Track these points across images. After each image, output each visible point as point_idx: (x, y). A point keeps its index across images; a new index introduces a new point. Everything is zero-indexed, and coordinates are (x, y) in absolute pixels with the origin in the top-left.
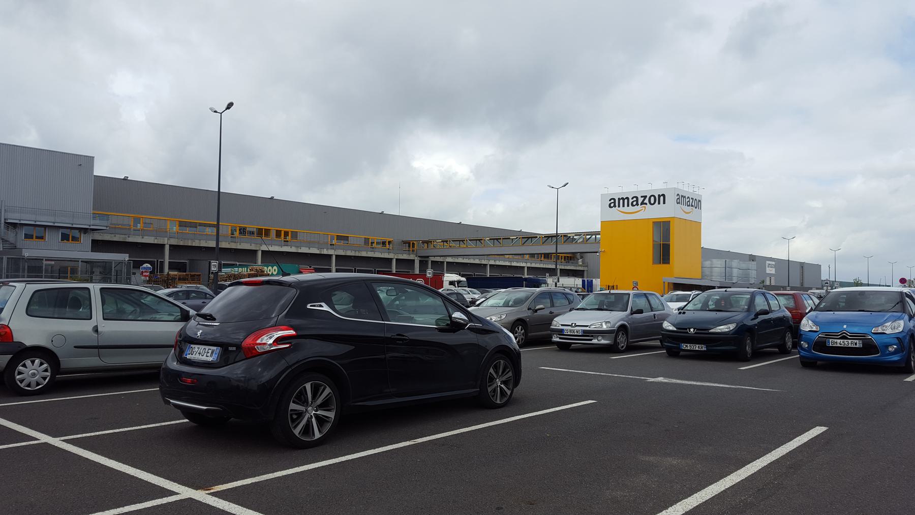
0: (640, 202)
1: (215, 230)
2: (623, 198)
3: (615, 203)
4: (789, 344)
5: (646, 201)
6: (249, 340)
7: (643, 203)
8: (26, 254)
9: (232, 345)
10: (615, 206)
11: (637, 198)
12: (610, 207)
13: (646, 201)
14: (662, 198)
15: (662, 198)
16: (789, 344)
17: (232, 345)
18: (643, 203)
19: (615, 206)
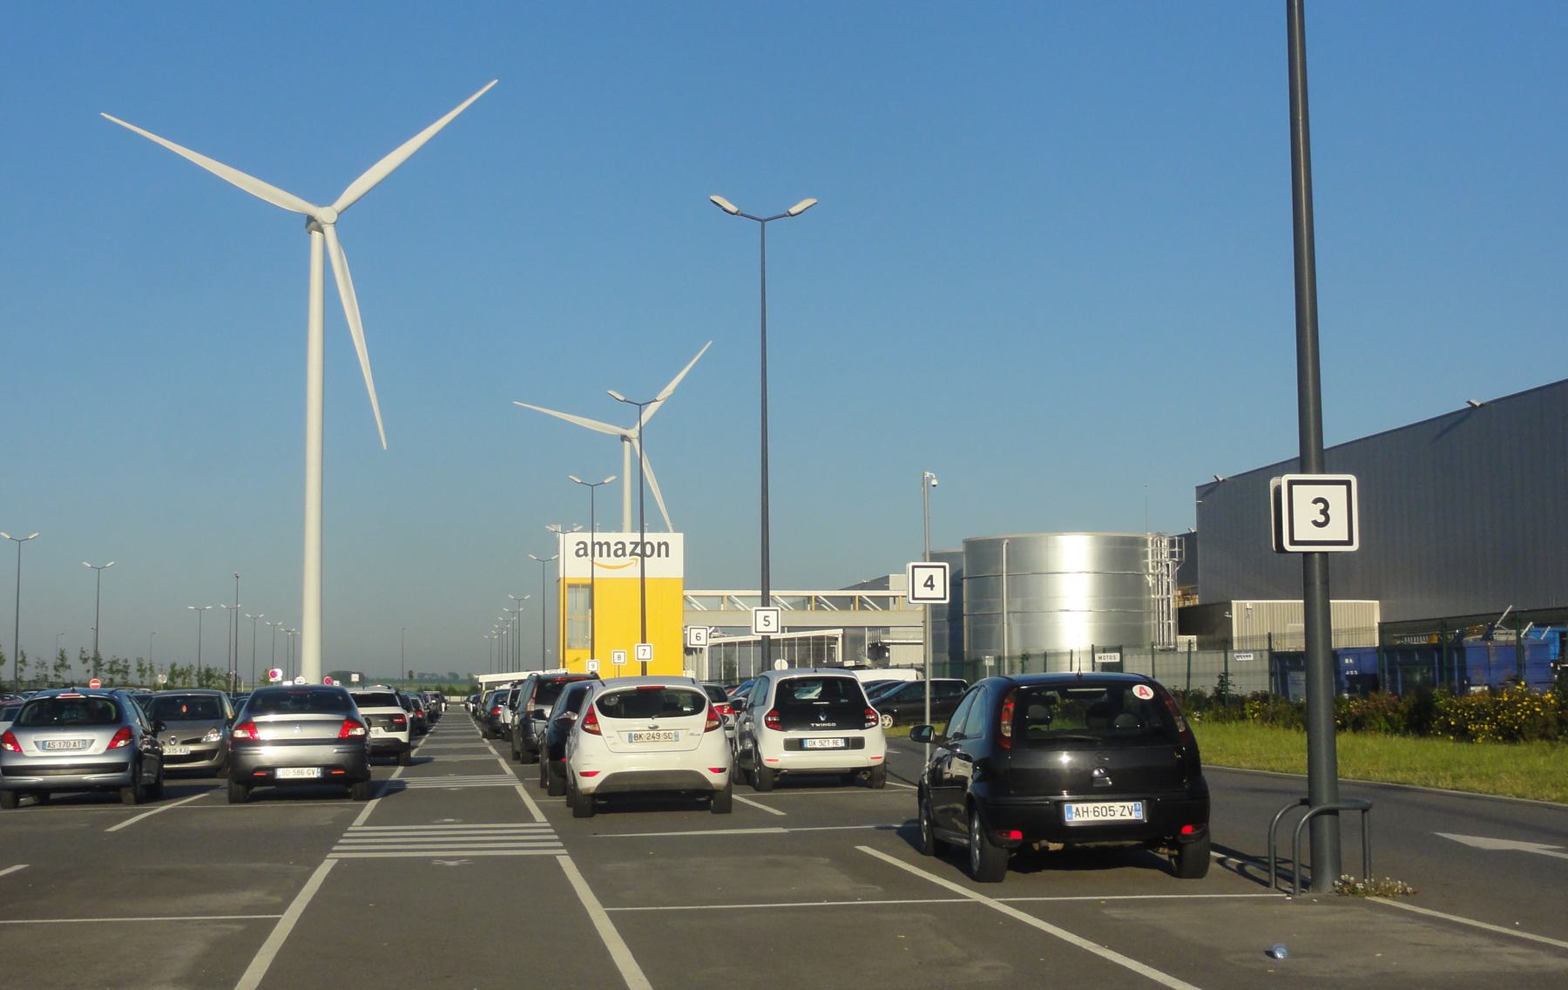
3: (585, 548)
10: (586, 554)
12: (577, 554)
18: (632, 553)
19: (586, 554)
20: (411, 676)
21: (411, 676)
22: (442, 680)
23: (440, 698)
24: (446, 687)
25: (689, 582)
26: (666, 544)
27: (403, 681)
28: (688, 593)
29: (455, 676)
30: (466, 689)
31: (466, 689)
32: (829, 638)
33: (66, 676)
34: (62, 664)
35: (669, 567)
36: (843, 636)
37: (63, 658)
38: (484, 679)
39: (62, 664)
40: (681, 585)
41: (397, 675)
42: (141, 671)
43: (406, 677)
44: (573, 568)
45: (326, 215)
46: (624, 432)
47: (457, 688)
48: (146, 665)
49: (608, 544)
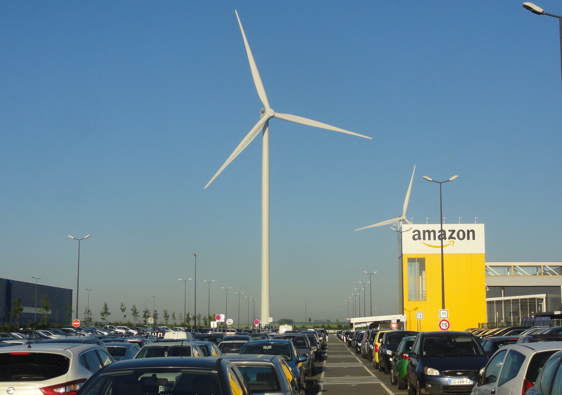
0: (447, 236)
1: (440, 249)
2: (428, 231)
3: (419, 234)
4: (302, 341)
5: (455, 235)
6: (289, 387)
7: (451, 237)
8: (24, 311)
9: (460, 375)
10: (419, 238)
11: (419, 232)
12: (414, 238)
13: (455, 235)
14: (471, 234)
15: (471, 234)
16: (302, 341)
17: (460, 375)
18: (451, 237)
19: (419, 238)
20: (310, 320)
21: (310, 320)
22: (324, 322)
23: (323, 333)
24: (326, 326)
25: (489, 256)
26: (473, 231)
27: (306, 323)
28: (488, 264)
29: (329, 321)
30: (336, 326)
31: (336, 326)
32: (538, 299)
33: (110, 319)
34: (106, 312)
35: (477, 246)
36: (546, 298)
37: (106, 308)
38: (353, 320)
39: (106, 312)
40: (483, 258)
41: (304, 321)
42: (166, 316)
43: (308, 321)
44: (411, 247)
45: (269, 112)
46: (400, 218)
47: (332, 326)
48: (170, 314)
49: (434, 232)
